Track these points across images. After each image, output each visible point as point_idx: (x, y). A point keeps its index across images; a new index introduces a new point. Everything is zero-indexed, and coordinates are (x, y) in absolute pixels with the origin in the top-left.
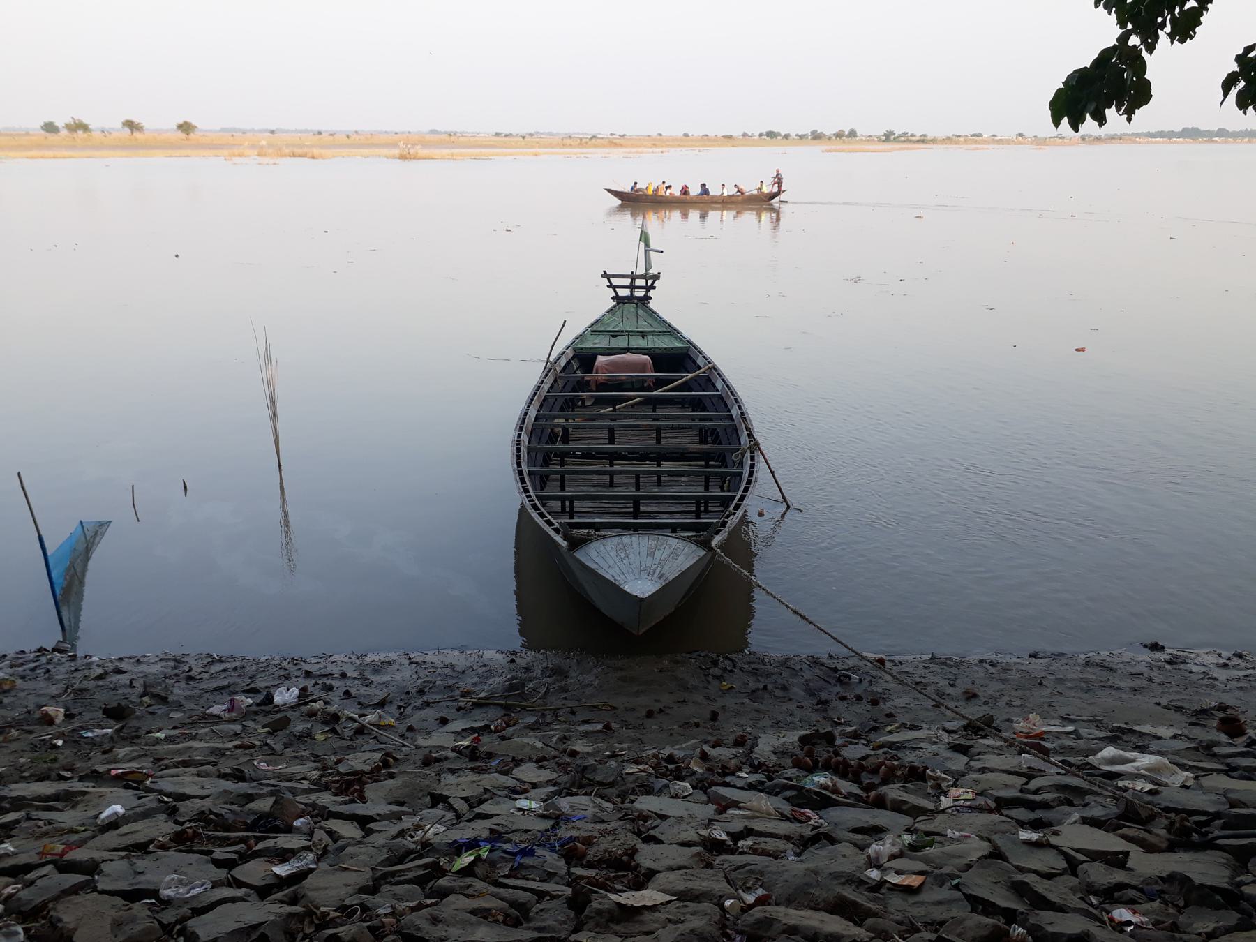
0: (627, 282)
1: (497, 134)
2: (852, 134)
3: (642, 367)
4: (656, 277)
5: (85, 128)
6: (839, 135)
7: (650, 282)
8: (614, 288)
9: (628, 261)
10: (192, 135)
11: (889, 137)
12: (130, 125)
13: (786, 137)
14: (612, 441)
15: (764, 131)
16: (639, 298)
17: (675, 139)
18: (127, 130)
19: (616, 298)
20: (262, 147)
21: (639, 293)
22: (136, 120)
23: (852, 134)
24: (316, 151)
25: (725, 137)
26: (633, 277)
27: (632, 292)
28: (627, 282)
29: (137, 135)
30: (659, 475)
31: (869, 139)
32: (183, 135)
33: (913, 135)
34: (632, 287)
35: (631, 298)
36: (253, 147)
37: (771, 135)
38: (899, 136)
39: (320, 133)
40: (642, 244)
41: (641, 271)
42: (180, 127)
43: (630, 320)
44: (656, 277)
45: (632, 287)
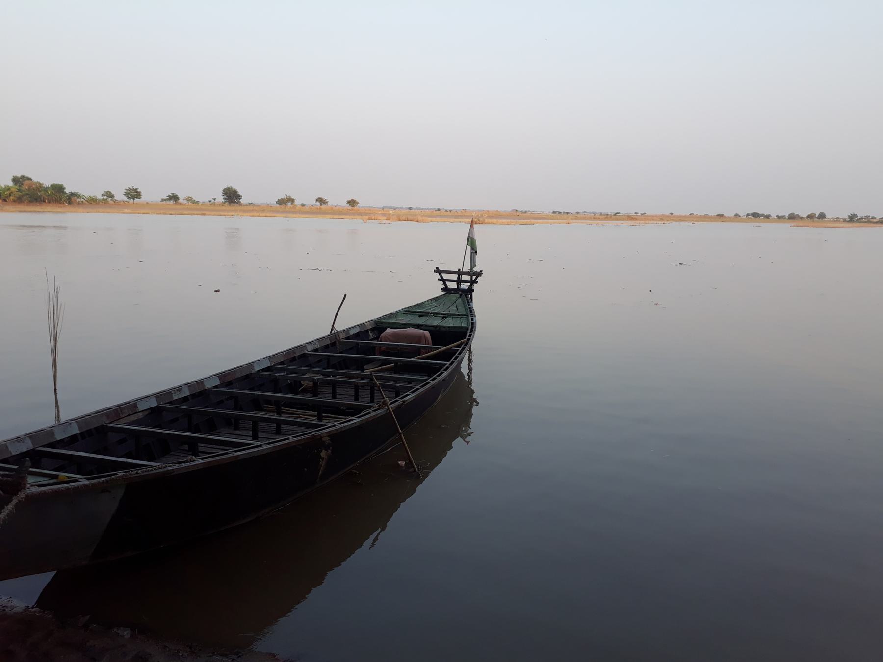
0: (455, 277)
1: (554, 212)
2: (822, 216)
3: (419, 339)
4: (479, 274)
5: (292, 200)
6: (811, 216)
7: (474, 277)
8: (442, 279)
9: (455, 259)
10: (355, 208)
11: (852, 219)
12: (321, 200)
13: (768, 217)
14: (356, 399)
15: (750, 212)
16: (464, 291)
17: (685, 217)
18: (318, 204)
19: (446, 289)
20: (389, 215)
21: (465, 286)
22: (324, 197)
23: (822, 216)
24: (420, 218)
25: (718, 215)
26: (460, 273)
27: (459, 285)
28: (455, 277)
29: (324, 207)
30: (279, 423)
31: (837, 220)
32: (350, 208)
33: (873, 218)
34: (459, 281)
35: (457, 290)
36: (384, 215)
37: (756, 215)
38: (862, 218)
39: (439, 210)
40: (469, 248)
41: (467, 269)
42: (349, 202)
43: (454, 306)
44: (479, 274)
45: (459, 281)
